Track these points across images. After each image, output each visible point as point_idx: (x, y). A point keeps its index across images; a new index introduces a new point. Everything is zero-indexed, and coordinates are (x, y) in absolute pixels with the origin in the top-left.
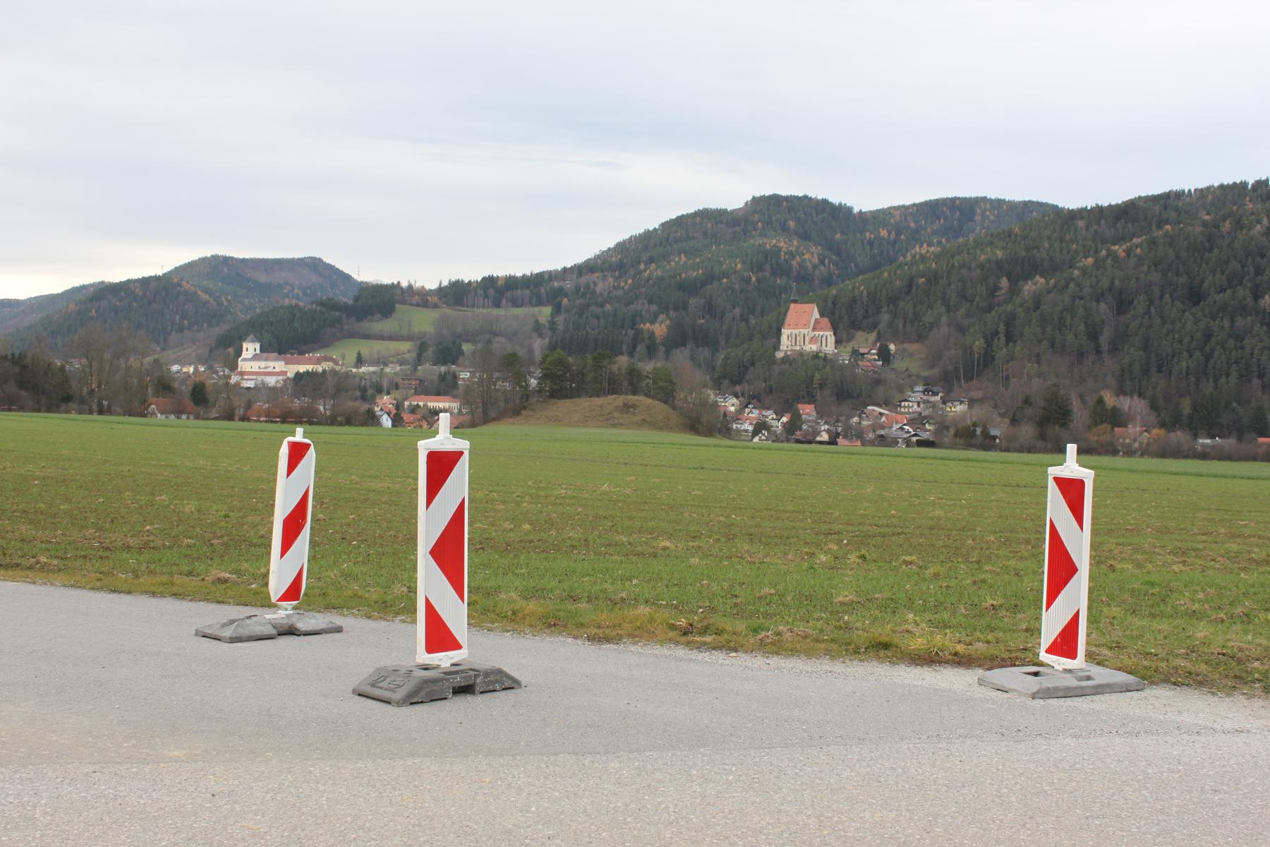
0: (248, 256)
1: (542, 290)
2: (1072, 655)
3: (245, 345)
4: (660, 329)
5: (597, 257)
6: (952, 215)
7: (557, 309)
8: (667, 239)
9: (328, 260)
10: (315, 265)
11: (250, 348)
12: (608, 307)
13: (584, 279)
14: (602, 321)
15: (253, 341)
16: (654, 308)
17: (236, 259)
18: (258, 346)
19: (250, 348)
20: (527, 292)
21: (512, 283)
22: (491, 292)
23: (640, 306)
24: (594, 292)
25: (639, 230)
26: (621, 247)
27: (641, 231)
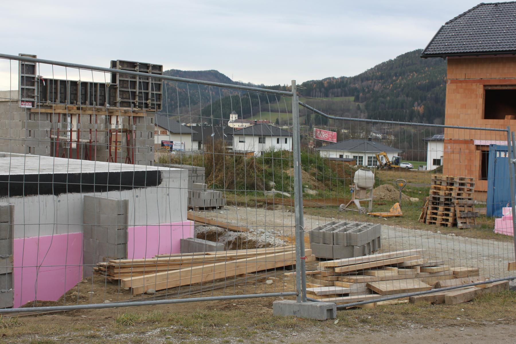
0: (186, 70)
1: (346, 89)
2: (34, 89)
3: (231, 116)
4: (420, 109)
5: (366, 72)
6: (398, 57)
7: (357, 99)
8: (403, 64)
9: (221, 71)
10: (215, 74)
11: (233, 117)
12: (388, 98)
13: (365, 83)
14: (387, 105)
15: (235, 114)
16: (410, 99)
17: (182, 71)
18: (237, 116)
19: (233, 117)
20: (339, 90)
21: (320, 84)
22: (323, 89)
23: (402, 98)
24: (373, 90)
25: (386, 60)
26: (379, 68)
27: (387, 60)
